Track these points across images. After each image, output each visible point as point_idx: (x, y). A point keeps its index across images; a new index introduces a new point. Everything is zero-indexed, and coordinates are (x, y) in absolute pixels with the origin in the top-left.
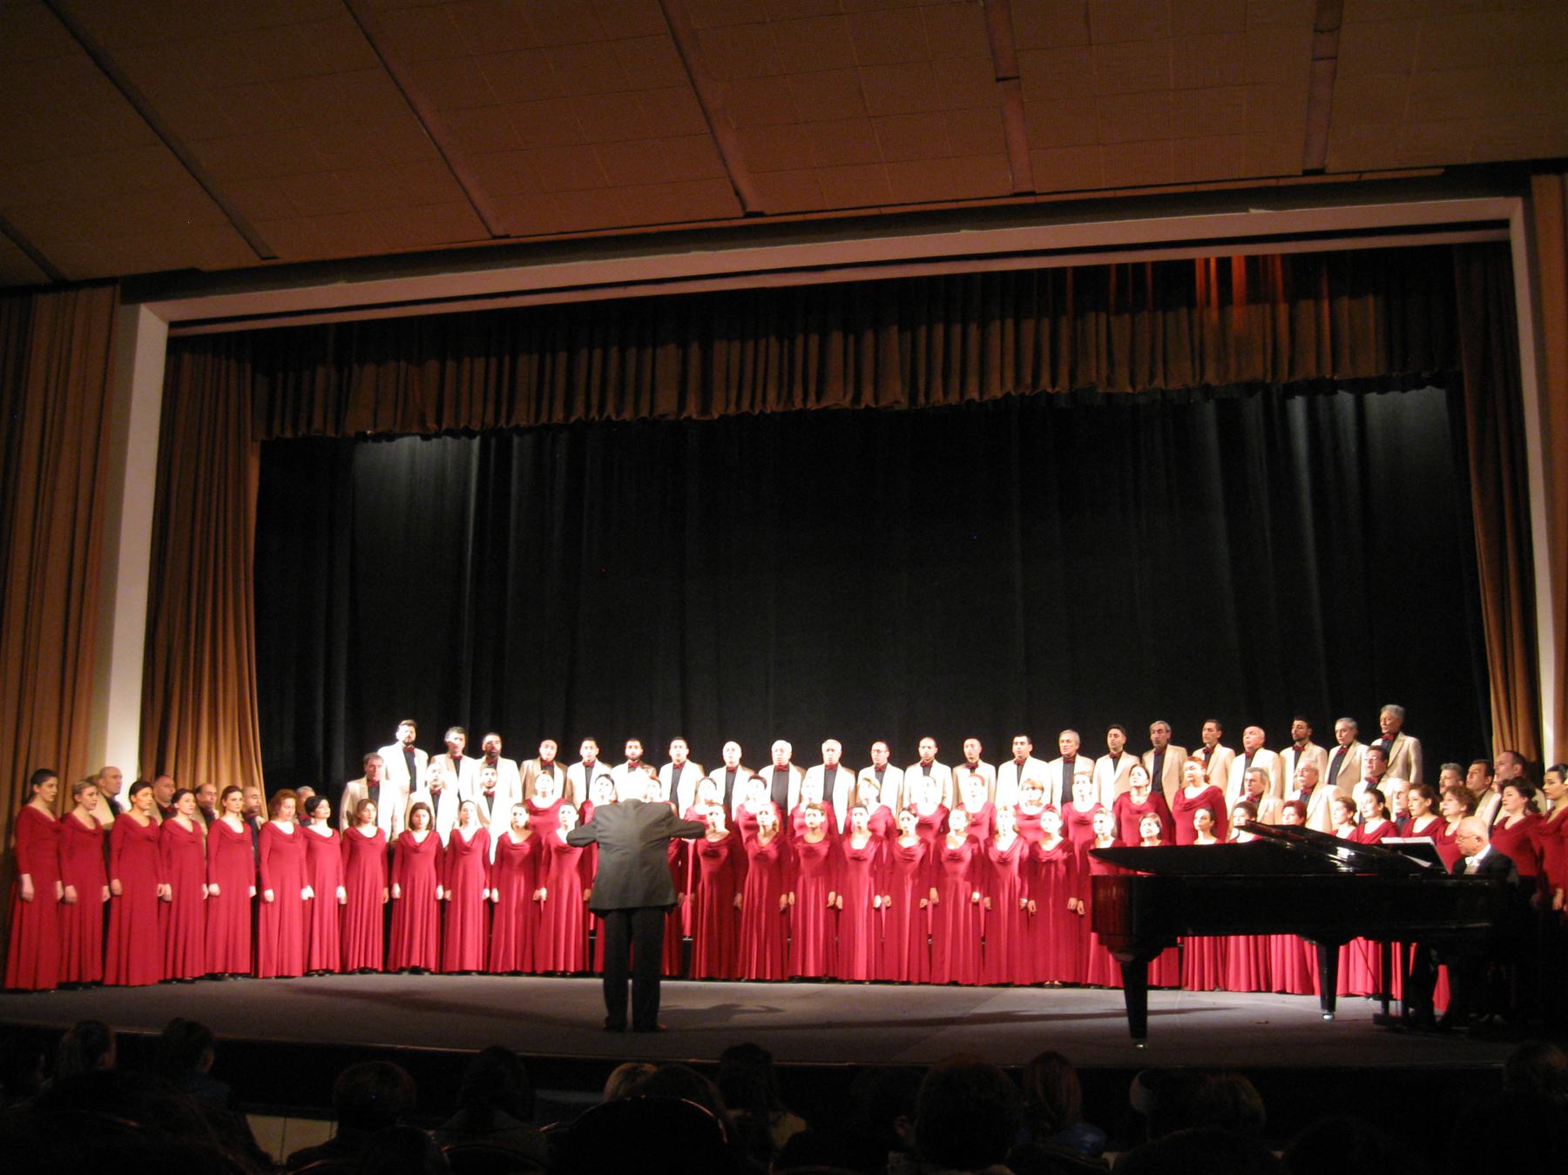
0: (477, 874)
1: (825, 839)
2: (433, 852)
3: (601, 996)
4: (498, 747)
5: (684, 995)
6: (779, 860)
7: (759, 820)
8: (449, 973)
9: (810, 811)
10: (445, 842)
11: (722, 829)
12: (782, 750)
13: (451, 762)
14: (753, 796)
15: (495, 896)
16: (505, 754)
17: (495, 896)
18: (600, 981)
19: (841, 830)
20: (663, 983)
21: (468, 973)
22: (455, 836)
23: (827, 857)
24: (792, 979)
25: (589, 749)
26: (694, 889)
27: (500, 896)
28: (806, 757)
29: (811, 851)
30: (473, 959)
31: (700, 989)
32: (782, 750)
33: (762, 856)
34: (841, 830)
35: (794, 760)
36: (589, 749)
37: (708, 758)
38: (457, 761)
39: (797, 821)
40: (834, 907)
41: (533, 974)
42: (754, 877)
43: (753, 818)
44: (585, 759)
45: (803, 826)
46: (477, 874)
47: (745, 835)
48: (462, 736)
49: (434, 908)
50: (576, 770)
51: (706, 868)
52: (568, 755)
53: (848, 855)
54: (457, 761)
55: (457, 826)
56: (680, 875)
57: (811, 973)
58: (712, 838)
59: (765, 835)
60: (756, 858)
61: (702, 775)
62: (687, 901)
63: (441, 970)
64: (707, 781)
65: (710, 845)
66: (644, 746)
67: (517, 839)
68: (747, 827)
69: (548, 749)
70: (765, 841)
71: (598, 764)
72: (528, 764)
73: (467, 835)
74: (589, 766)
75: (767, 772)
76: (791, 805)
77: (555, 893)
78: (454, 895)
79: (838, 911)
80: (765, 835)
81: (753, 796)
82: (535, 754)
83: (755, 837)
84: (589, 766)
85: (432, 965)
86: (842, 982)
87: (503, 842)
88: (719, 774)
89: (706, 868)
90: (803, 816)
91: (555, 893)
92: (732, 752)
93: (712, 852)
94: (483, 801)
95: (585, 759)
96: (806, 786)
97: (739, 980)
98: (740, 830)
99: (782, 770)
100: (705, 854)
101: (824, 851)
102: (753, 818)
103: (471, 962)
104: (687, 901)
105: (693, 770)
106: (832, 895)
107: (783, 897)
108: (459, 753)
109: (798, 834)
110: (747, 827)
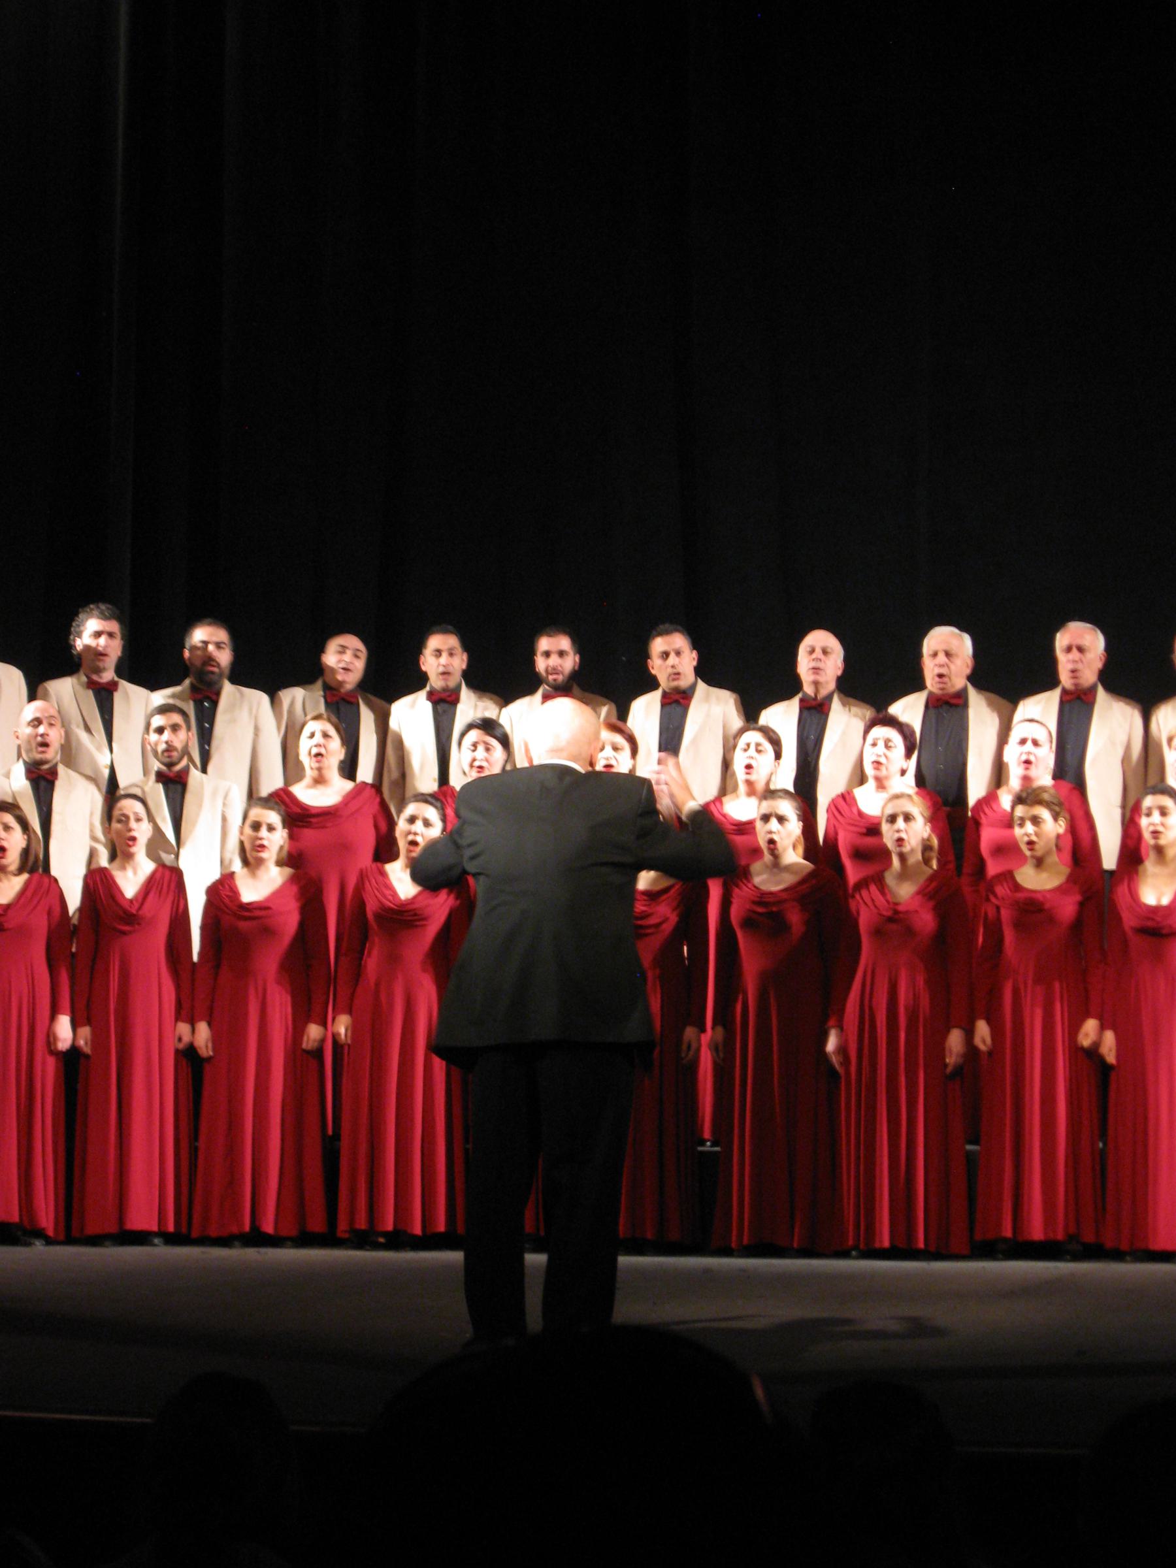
0: (155, 989)
1: (1072, 879)
2: (40, 925)
3: (461, 1295)
4: (224, 658)
5: (663, 1285)
6: (941, 937)
7: (888, 835)
8: (94, 1241)
9: (1020, 811)
10: (74, 899)
11: (793, 856)
12: (947, 650)
13: (89, 697)
14: (871, 766)
15: (203, 1035)
16: (242, 675)
17: (203, 1035)
18: (456, 1257)
19: (1109, 858)
20: (623, 1260)
21: (140, 1238)
22: (98, 884)
23: (1077, 925)
24: (987, 1250)
25: (442, 656)
26: (723, 1017)
27: (216, 1038)
28: (1011, 670)
29: (1031, 908)
30: (147, 1201)
31: (745, 1276)
32: (947, 650)
33: (895, 920)
34: (1109, 858)
35: (981, 678)
36: (442, 656)
37: (757, 678)
38: (104, 696)
39: (988, 836)
40: (1093, 1053)
41: (329, 1240)
42: (881, 982)
43: (873, 829)
44: (435, 682)
45: (1008, 849)
46: (155, 989)
47: (853, 873)
48: (114, 626)
49: (48, 1072)
50: (412, 716)
51: (753, 962)
52: (392, 676)
53: (1129, 921)
54: (104, 696)
55: (103, 861)
56: (683, 985)
57: (1037, 1231)
58: (763, 880)
59: (904, 875)
60: (878, 932)
61: (737, 722)
62: (704, 1043)
63: (71, 1233)
64: (753, 737)
65: (763, 898)
66: (580, 646)
67: (253, 890)
68: (860, 855)
69: (344, 656)
70: (905, 891)
71: (466, 695)
72: (295, 696)
73: (130, 881)
74: (444, 703)
75: (910, 709)
76: (976, 790)
77: (372, 1029)
78: (98, 1040)
79: (1104, 1070)
80: (904, 875)
81: (871, 766)
82: (308, 671)
83: (878, 880)
84: (444, 703)
85: (47, 1216)
86: (1117, 1255)
87: (222, 894)
88: (782, 717)
89: (753, 962)
90: (1008, 822)
91: (372, 1029)
92: (820, 655)
93: (767, 915)
94: (158, 795)
95: (435, 682)
96: (1007, 746)
97: (844, 1254)
98: (843, 858)
99: (947, 710)
100: (749, 923)
101: (1068, 908)
102: (873, 829)
103: (147, 1201)
104: (704, 1043)
105: (713, 709)
106: (1090, 1027)
107: (955, 1040)
108: (108, 675)
109: (993, 868)
110: (860, 855)
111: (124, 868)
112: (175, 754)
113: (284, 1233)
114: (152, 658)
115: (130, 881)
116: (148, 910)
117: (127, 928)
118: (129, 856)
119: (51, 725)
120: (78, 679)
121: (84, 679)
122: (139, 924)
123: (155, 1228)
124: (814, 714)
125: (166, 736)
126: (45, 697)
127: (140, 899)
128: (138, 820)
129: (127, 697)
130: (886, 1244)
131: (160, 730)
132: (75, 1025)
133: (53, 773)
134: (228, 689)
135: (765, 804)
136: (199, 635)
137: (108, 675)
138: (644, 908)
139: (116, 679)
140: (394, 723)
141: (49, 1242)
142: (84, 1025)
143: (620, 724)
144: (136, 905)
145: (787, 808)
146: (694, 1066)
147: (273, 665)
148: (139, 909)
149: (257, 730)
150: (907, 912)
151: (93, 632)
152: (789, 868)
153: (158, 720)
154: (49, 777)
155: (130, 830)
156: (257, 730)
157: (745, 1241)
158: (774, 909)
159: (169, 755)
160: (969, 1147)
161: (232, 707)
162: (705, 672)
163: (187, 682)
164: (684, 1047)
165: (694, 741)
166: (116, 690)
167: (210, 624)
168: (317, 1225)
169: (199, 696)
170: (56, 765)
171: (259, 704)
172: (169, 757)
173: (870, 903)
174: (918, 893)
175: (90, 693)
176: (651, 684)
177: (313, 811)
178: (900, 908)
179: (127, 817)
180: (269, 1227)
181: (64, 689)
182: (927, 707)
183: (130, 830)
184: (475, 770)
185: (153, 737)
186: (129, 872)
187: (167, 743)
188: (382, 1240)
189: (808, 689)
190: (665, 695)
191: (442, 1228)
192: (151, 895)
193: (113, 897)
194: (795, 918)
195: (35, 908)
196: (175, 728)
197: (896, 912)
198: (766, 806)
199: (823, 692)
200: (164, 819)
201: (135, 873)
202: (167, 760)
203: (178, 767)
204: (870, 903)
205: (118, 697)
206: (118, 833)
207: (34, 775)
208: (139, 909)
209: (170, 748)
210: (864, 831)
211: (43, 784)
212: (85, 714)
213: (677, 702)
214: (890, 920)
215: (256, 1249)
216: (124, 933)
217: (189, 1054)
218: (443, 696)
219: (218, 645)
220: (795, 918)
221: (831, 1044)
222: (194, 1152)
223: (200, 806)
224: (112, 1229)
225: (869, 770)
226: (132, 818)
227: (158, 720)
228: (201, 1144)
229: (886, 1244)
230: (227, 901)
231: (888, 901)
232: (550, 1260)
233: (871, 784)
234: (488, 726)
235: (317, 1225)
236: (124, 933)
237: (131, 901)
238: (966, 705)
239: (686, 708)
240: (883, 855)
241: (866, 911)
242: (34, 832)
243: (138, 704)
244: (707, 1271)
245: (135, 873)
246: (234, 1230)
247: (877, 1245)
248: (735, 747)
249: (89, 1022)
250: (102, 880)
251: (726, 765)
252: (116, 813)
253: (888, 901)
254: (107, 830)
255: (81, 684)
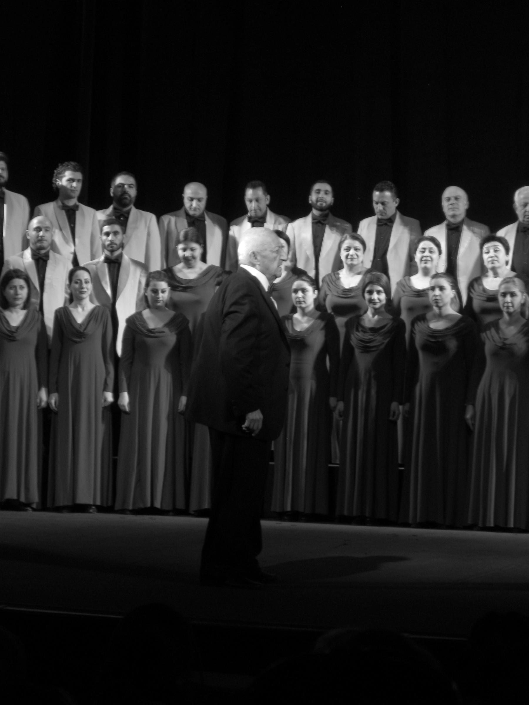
4: (133, 192)
8: (59, 509)
11: (451, 310)
16: (142, 204)
18: (205, 521)
21: (83, 508)
22: (63, 317)
30: (88, 490)
35: (210, 207)
41: (185, 512)
48: (79, 176)
54: (71, 214)
60: (495, 354)
65: (434, 334)
73: (80, 315)
78: (62, 401)
83: (496, 325)
85: (35, 497)
88: (439, 232)
92: (455, 200)
93: (435, 344)
111: (76, 307)
112: (115, 246)
113: (166, 508)
114: (96, 194)
115: (80, 315)
116: (89, 331)
117: (78, 340)
118: (80, 300)
119: (47, 230)
120: (57, 203)
121: (60, 203)
122: (84, 338)
123: (92, 503)
124: (454, 232)
125: (110, 238)
126: (39, 214)
127: (85, 324)
128: (87, 282)
129: (83, 214)
130: (492, 525)
131: (107, 234)
132: (49, 393)
133: (47, 256)
134: (134, 212)
135: (434, 281)
136: (119, 180)
137: (72, 202)
138: (370, 337)
139: (78, 203)
140: (231, 233)
141: (34, 510)
142: (54, 392)
143: (353, 234)
144: (83, 327)
145: (445, 282)
146: (395, 423)
147: (161, 200)
148: (85, 329)
149: (149, 234)
150: (510, 344)
151: (67, 178)
152: (448, 317)
153: (106, 228)
154: (44, 258)
155: (83, 288)
156: (149, 234)
157: (418, 520)
158: (440, 340)
159: (111, 248)
160: (403, 468)
161: (136, 221)
162: (403, 209)
163: (111, 209)
164: (391, 413)
165: (396, 246)
166: (77, 210)
167: (125, 174)
168: (180, 504)
169: (118, 214)
170: (48, 252)
171: (151, 220)
172: (112, 247)
173: (491, 338)
174: (519, 332)
175: (64, 212)
176: (370, 213)
177: (178, 279)
178: (507, 342)
179: (81, 281)
180: (158, 505)
181: (49, 209)
182: (518, 231)
183: (83, 288)
184: (349, 260)
185: (104, 237)
186: (80, 309)
187: (110, 241)
188: (93, 507)
189: (521, 219)
190: (379, 220)
191: (355, 513)
192: (92, 322)
193: (71, 324)
194: (452, 344)
195: (32, 328)
196: (116, 233)
197: (505, 344)
198: (434, 282)
199: (459, 219)
200: (106, 283)
201: (83, 309)
202: (110, 249)
203: (117, 253)
204: (491, 338)
205: (78, 213)
206: (76, 289)
207: (37, 257)
208: (85, 329)
209: (112, 243)
210: (485, 299)
211: (41, 261)
212: (60, 223)
213: (386, 224)
214: (502, 348)
215: (150, 516)
216: (76, 342)
217: (114, 408)
218: (256, 219)
219: (130, 186)
220: (452, 344)
221: (468, 416)
222: (115, 463)
223: (128, 276)
224: (70, 504)
225: (489, 266)
226: (83, 281)
227: (106, 228)
228: (121, 457)
229: (492, 525)
230: (140, 327)
231: (500, 338)
232: (210, 523)
233: (490, 273)
234: (280, 234)
235: (180, 504)
236: (76, 342)
237: (81, 325)
238: (204, 221)
239: (391, 227)
240: (498, 311)
241: (490, 340)
242: (35, 288)
243: (93, 220)
244: (395, 536)
245: (83, 309)
246: (142, 506)
247: (488, 525)
248: (416, 249)
249: (57, 390)
250: (64, 314)
251: (411, 258)
252: (74, 279)
253: (500, 338)
254: (70, 285)
255: (59, 207)
